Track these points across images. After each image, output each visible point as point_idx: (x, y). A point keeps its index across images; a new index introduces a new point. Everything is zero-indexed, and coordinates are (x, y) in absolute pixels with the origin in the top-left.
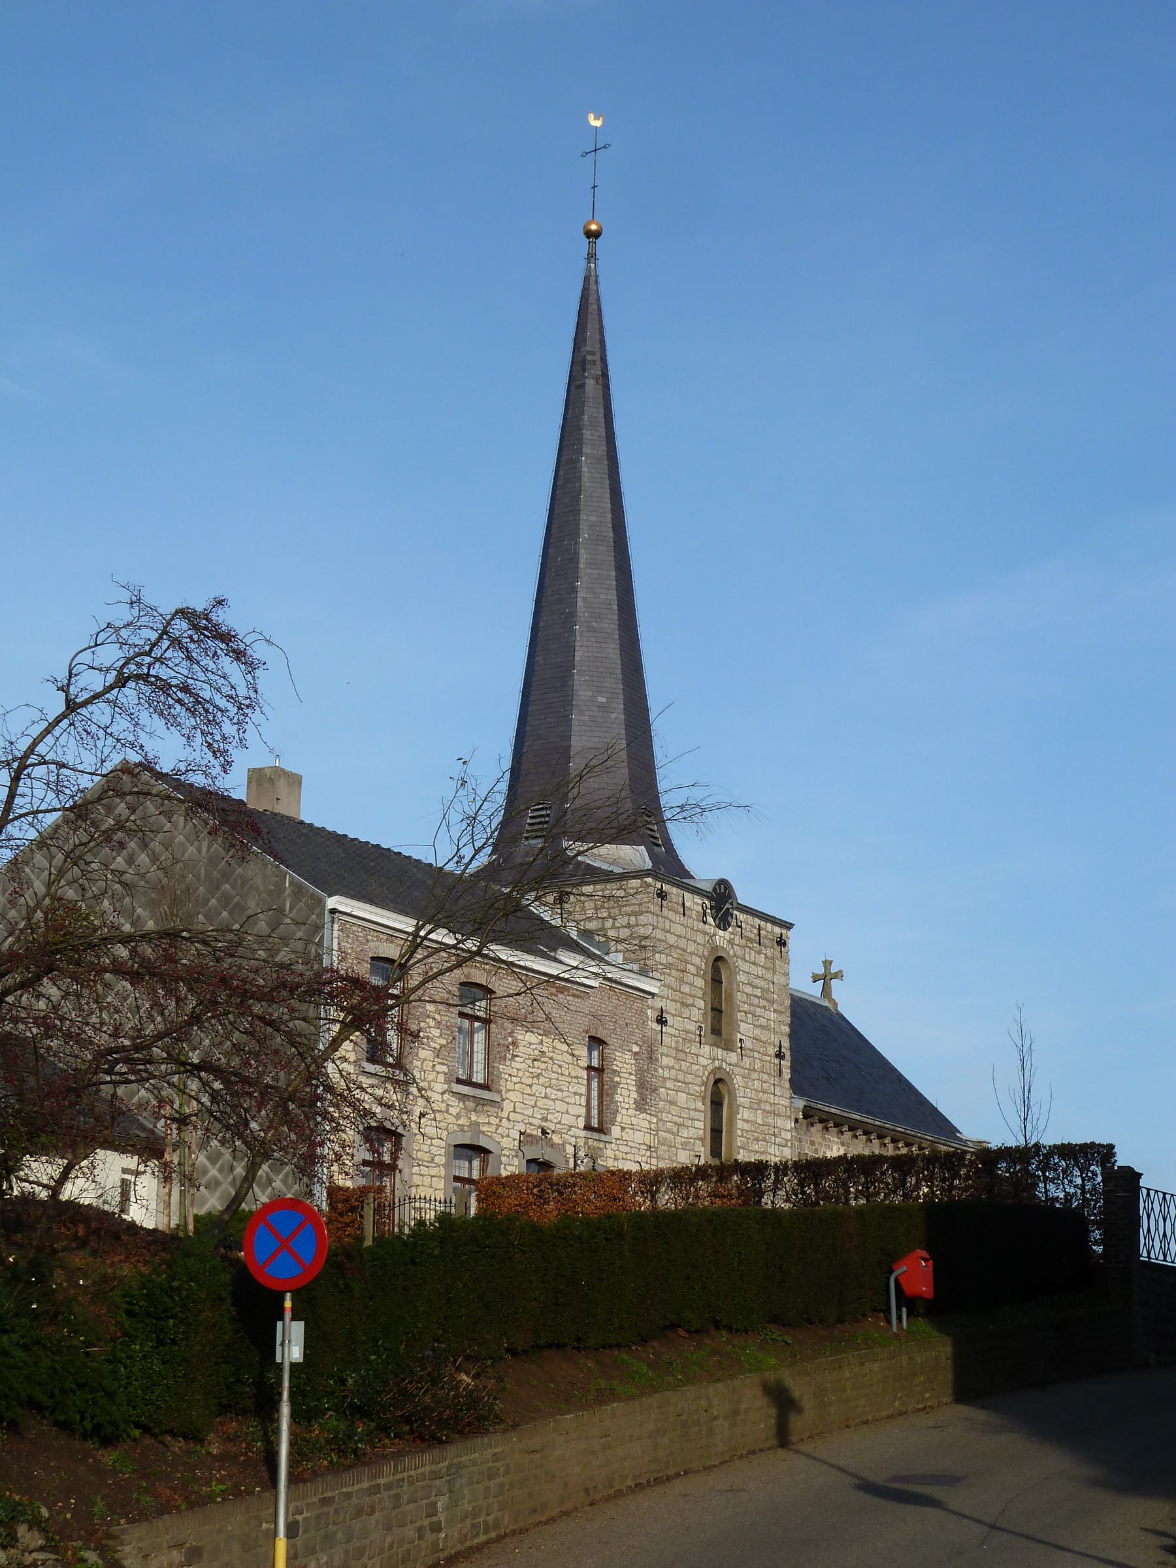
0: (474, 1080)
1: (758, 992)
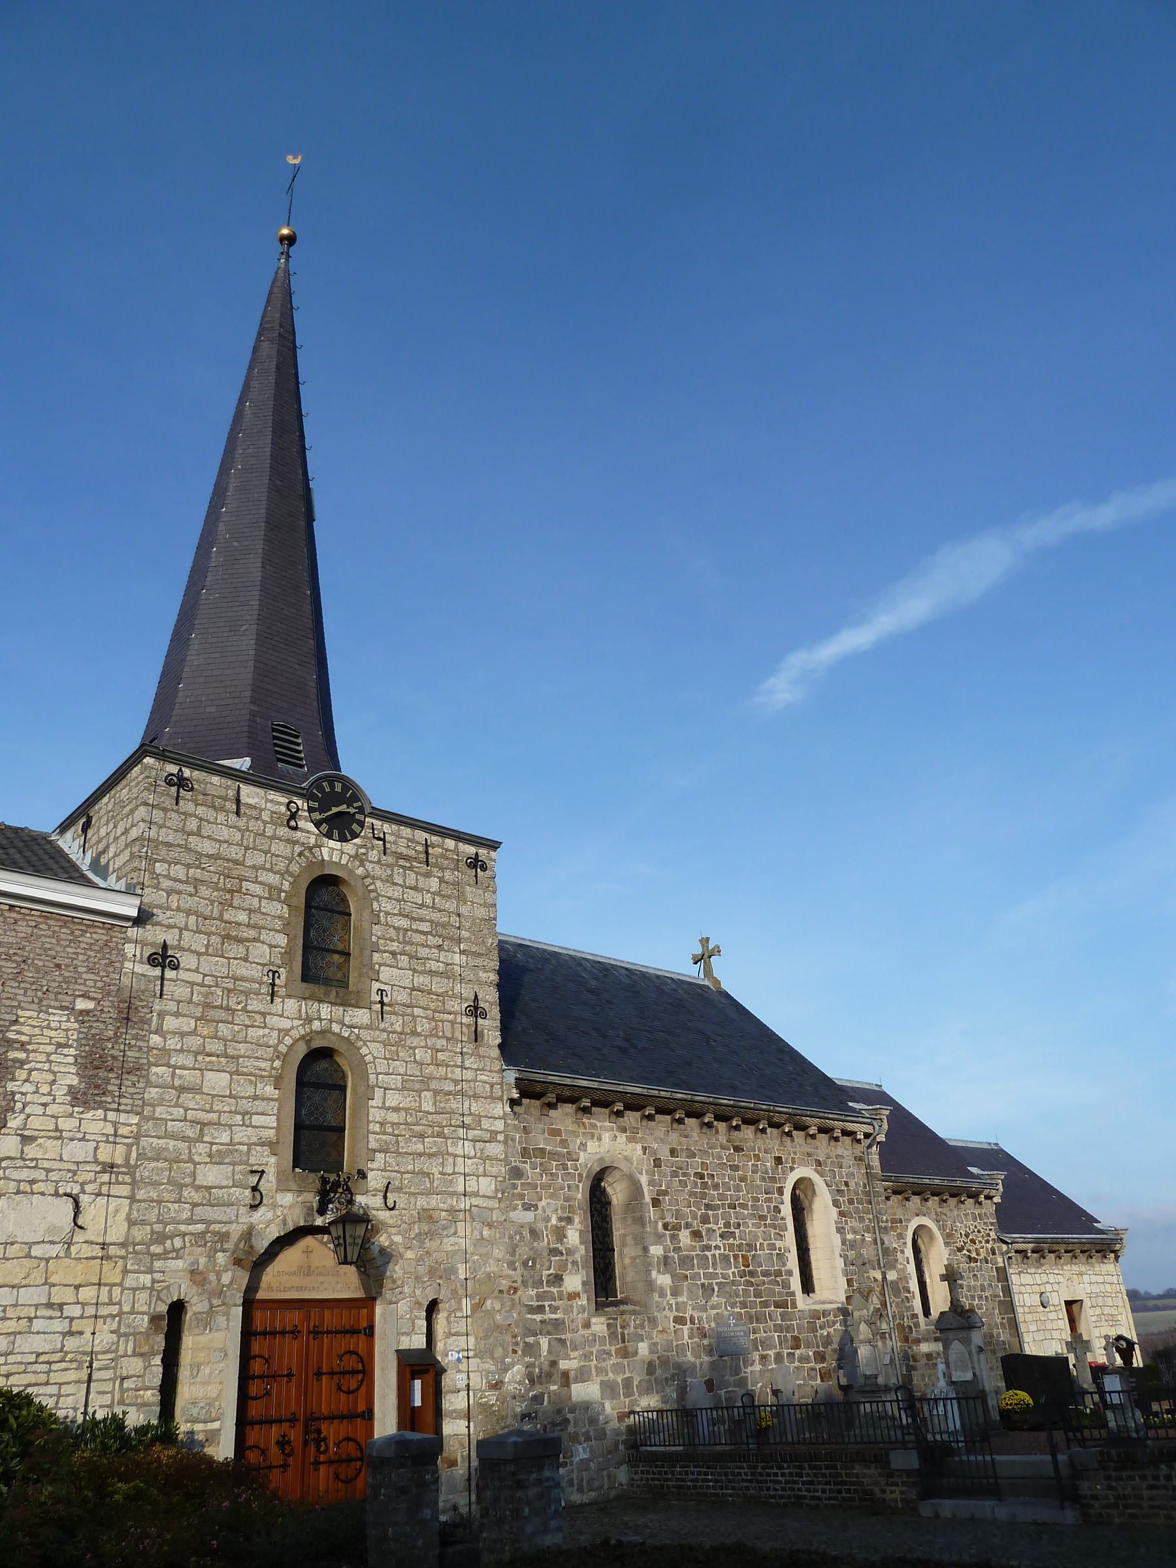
0: (275, 1125)
1: (425, 927)
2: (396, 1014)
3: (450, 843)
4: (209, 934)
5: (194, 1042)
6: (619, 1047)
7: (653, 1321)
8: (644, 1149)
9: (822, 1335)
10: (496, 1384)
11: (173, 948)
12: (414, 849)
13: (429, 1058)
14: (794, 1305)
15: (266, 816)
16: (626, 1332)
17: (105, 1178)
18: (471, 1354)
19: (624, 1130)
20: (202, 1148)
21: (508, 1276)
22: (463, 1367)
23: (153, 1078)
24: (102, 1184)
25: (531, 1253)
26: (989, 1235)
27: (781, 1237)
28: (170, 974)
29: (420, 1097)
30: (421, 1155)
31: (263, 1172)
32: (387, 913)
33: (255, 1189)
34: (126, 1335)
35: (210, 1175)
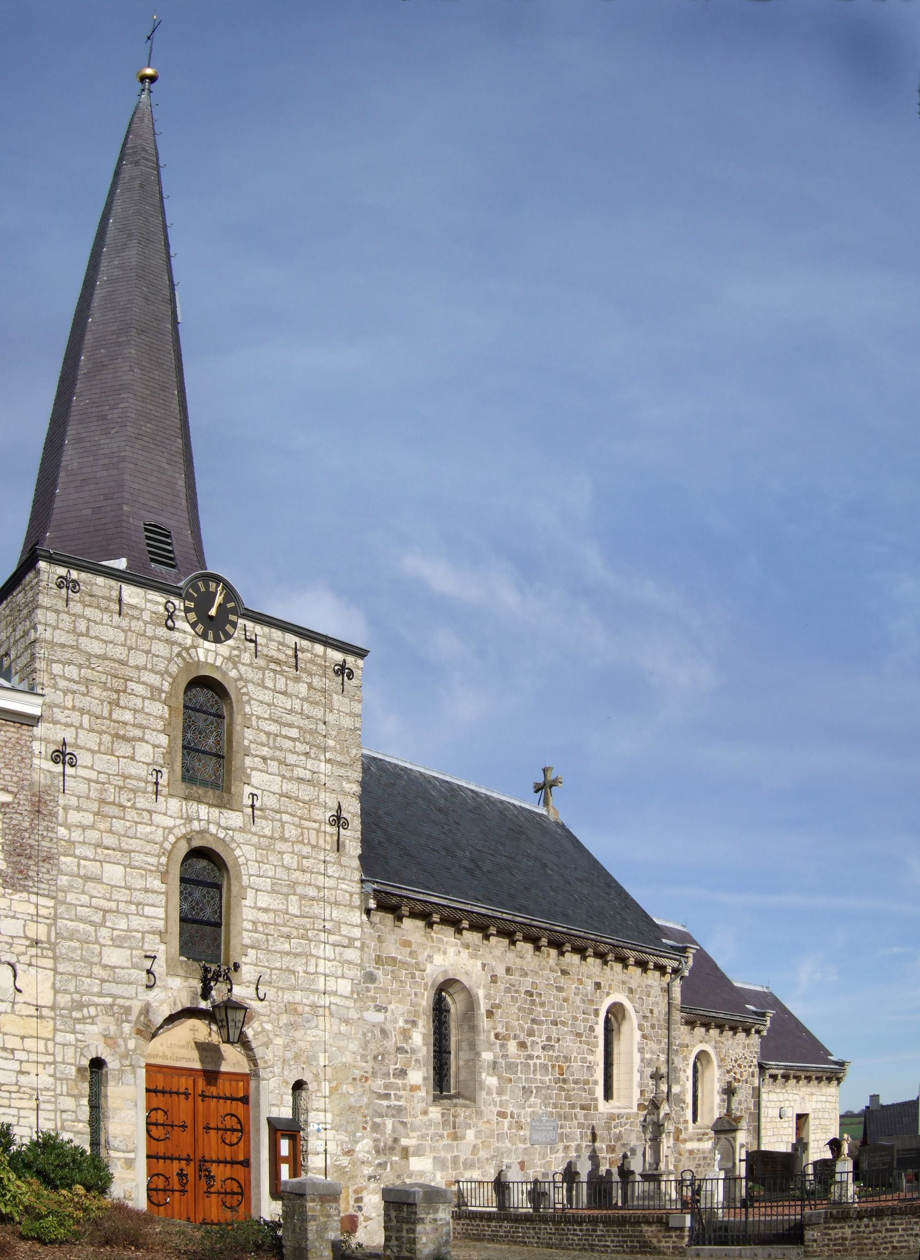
0: (163, 916)
1: (294, 733)
2: (265, 818)
3: (319, 648)
4: (101, 733)
5: (93, 835)
6: (465, 867)
7: (479, 1113)
8: (484, 965)
9: (615, 1133)
10: (349, 1152)
11: (72, 746)
12: (284, 653)
13: (296, 863)
14: (596, 1108)
15: (146, 616)
16: (457, 1120)
17: (33, 951)
18: (328, 1126)
19: (467, 946)
20: (104, 932)
21: (362, 1068)
22: (322, 1135)
23: (63, 867)
24: (32, 956)
25: (381, 1049)
26: (752, 1061)
27: (592, 1052)
28: (69, 770)
29: (287, 901)
30: (288, 954)
31: (155, 957)
32: (258, 718)
33: (149, 972)
34: (61, 1079)
35: (114, 956)
